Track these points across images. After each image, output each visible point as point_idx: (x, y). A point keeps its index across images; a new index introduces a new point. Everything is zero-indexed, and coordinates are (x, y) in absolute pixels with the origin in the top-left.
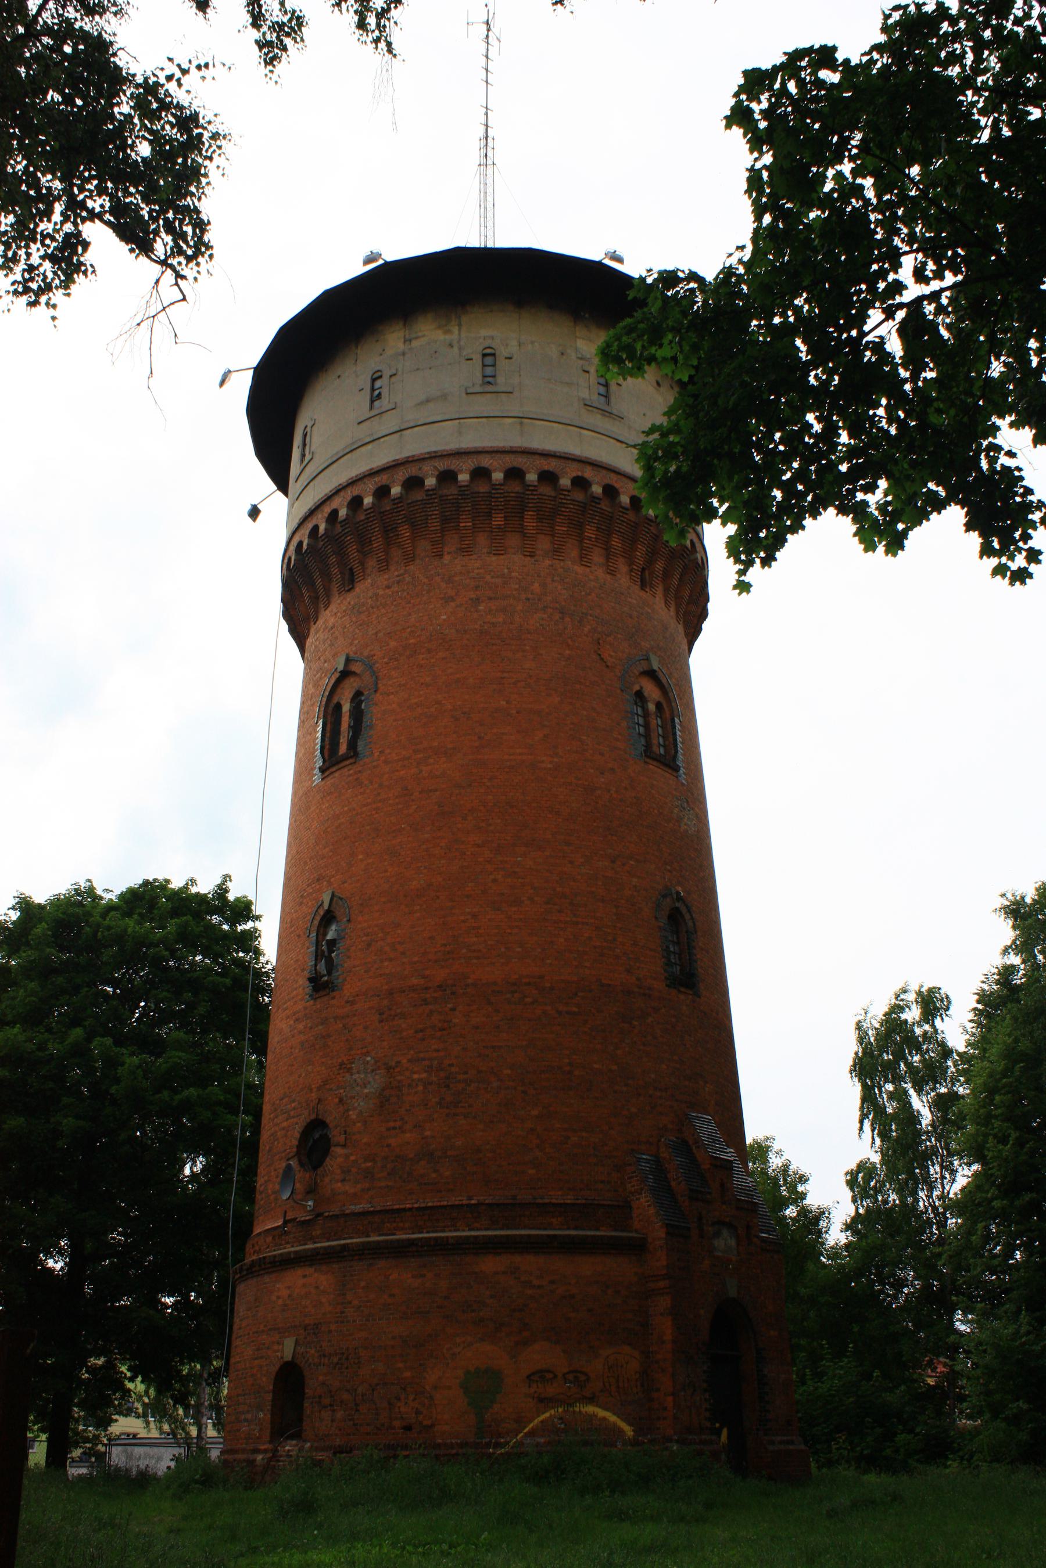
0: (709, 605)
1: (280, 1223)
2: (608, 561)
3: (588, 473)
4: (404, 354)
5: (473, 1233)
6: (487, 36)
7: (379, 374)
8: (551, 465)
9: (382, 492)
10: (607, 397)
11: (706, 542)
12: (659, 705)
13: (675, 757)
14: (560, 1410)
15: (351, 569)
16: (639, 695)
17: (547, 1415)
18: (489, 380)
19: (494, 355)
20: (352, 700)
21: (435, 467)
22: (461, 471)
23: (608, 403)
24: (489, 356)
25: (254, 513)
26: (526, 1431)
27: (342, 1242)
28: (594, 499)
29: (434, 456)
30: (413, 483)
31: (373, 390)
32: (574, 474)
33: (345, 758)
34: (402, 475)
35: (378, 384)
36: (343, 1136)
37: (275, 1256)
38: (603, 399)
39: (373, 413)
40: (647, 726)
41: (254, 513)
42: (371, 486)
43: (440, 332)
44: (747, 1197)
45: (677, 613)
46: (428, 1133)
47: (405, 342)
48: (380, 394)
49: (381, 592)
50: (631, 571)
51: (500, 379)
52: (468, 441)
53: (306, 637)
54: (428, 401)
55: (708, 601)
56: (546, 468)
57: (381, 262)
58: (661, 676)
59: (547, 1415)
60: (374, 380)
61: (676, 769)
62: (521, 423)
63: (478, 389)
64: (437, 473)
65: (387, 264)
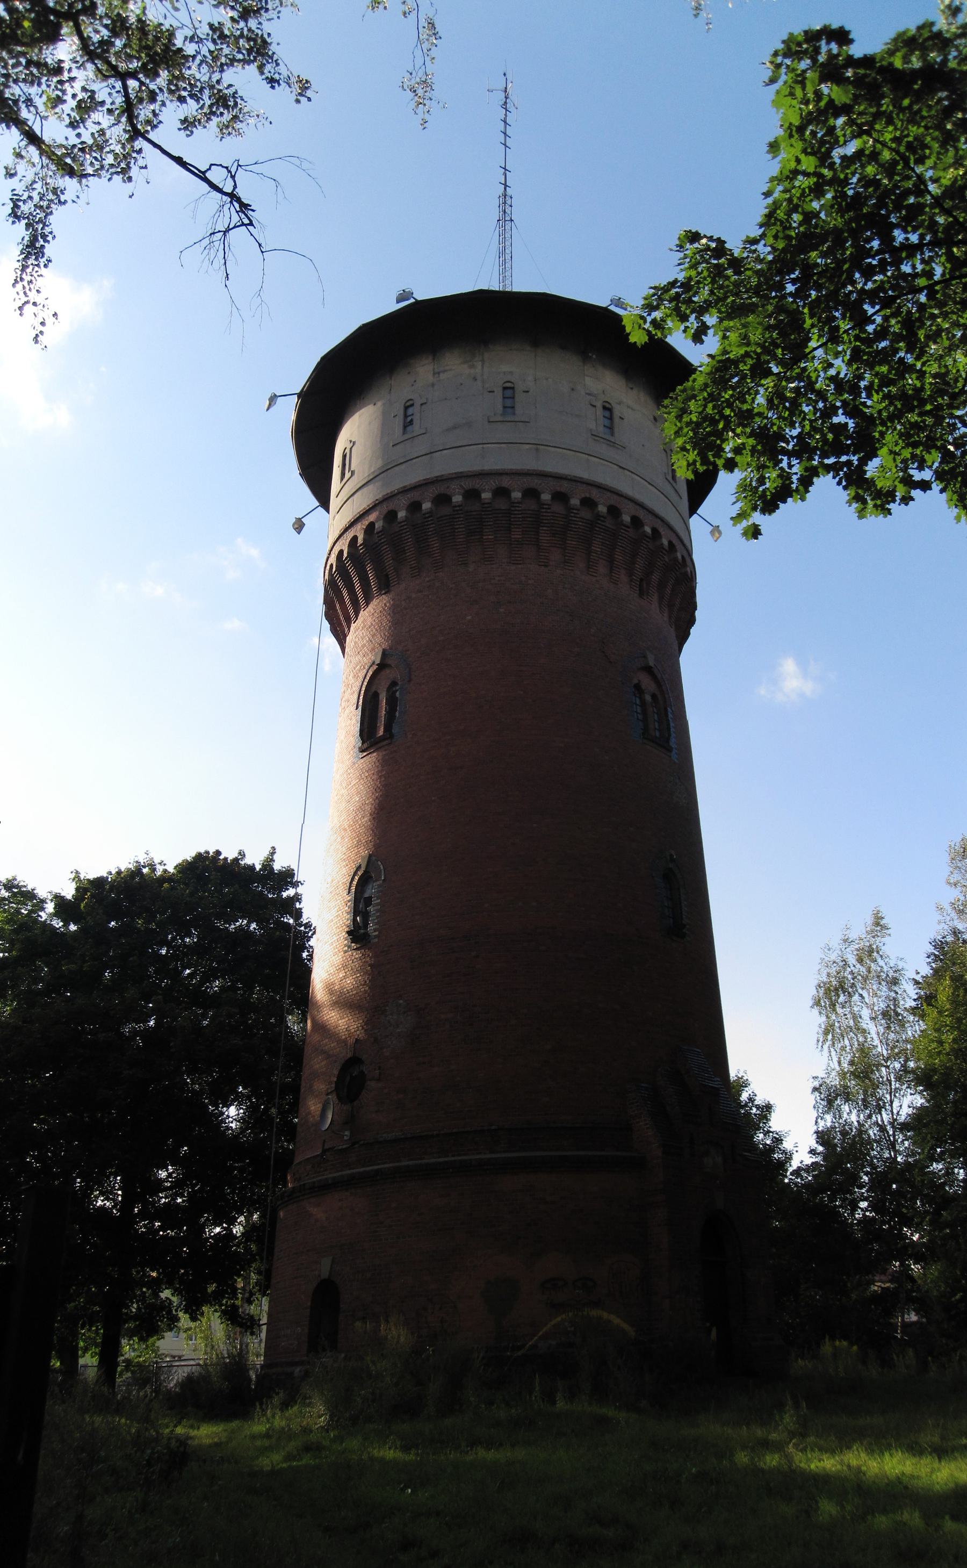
0: (697, 613)
1: (319, 1152)
2: (611, 572)
3: (595, 494)
4: (433, 385)
5: (494, 1156)
6: (506, 102)
7: (411, 402)
8: (564, 487)
9: (415, 507)
10: (611, 428)
11: (694, 557)
12: (654, 696)
13: (668, 740)
14: (570, 1314)
15: (387, 575)
16: (638, 687)
17: (559, 1319)
18: (509, 408)
19: (513, 388)
20: (388, 690)
21: (461, 486)
22: (484, 491)
23: (612, 434)
24: (509, 390)
25: (299, 526)
26: (541, 1333)
27: (376, 1167)
28: (598, 516)
29: (460, 476)
30: (443, 500)
31: (406, 416)
32: (583, 496)
33: (383, 738)
34: (433, 491)
35: (410, 411)
36: (377, 1071)
37: (314, 1183)
38: (607, 430)
39: (406, 437)
40: (644, 712)
41: (299, 526)
42: (404, 501)
43: (466, 366)
44: (729, 1119)
45: (670, 617)
46: (105, 33)
47: (434, 374)
48: (412, 420)
49: (414, 595)
50: (631, 581)
51: (519, 410)
52: (491, 464)
53: (345, 636)
54: (455, 428)
55: (695, 609)
56: (558, 489)
57: (412, 301)
58: (656, 671)
59: (559, 1319)
60: (406, 408)
61: (670, 750)
62: (537, 450)
63: (500, 419)
64: (462, 491)
65: (417, 303)
